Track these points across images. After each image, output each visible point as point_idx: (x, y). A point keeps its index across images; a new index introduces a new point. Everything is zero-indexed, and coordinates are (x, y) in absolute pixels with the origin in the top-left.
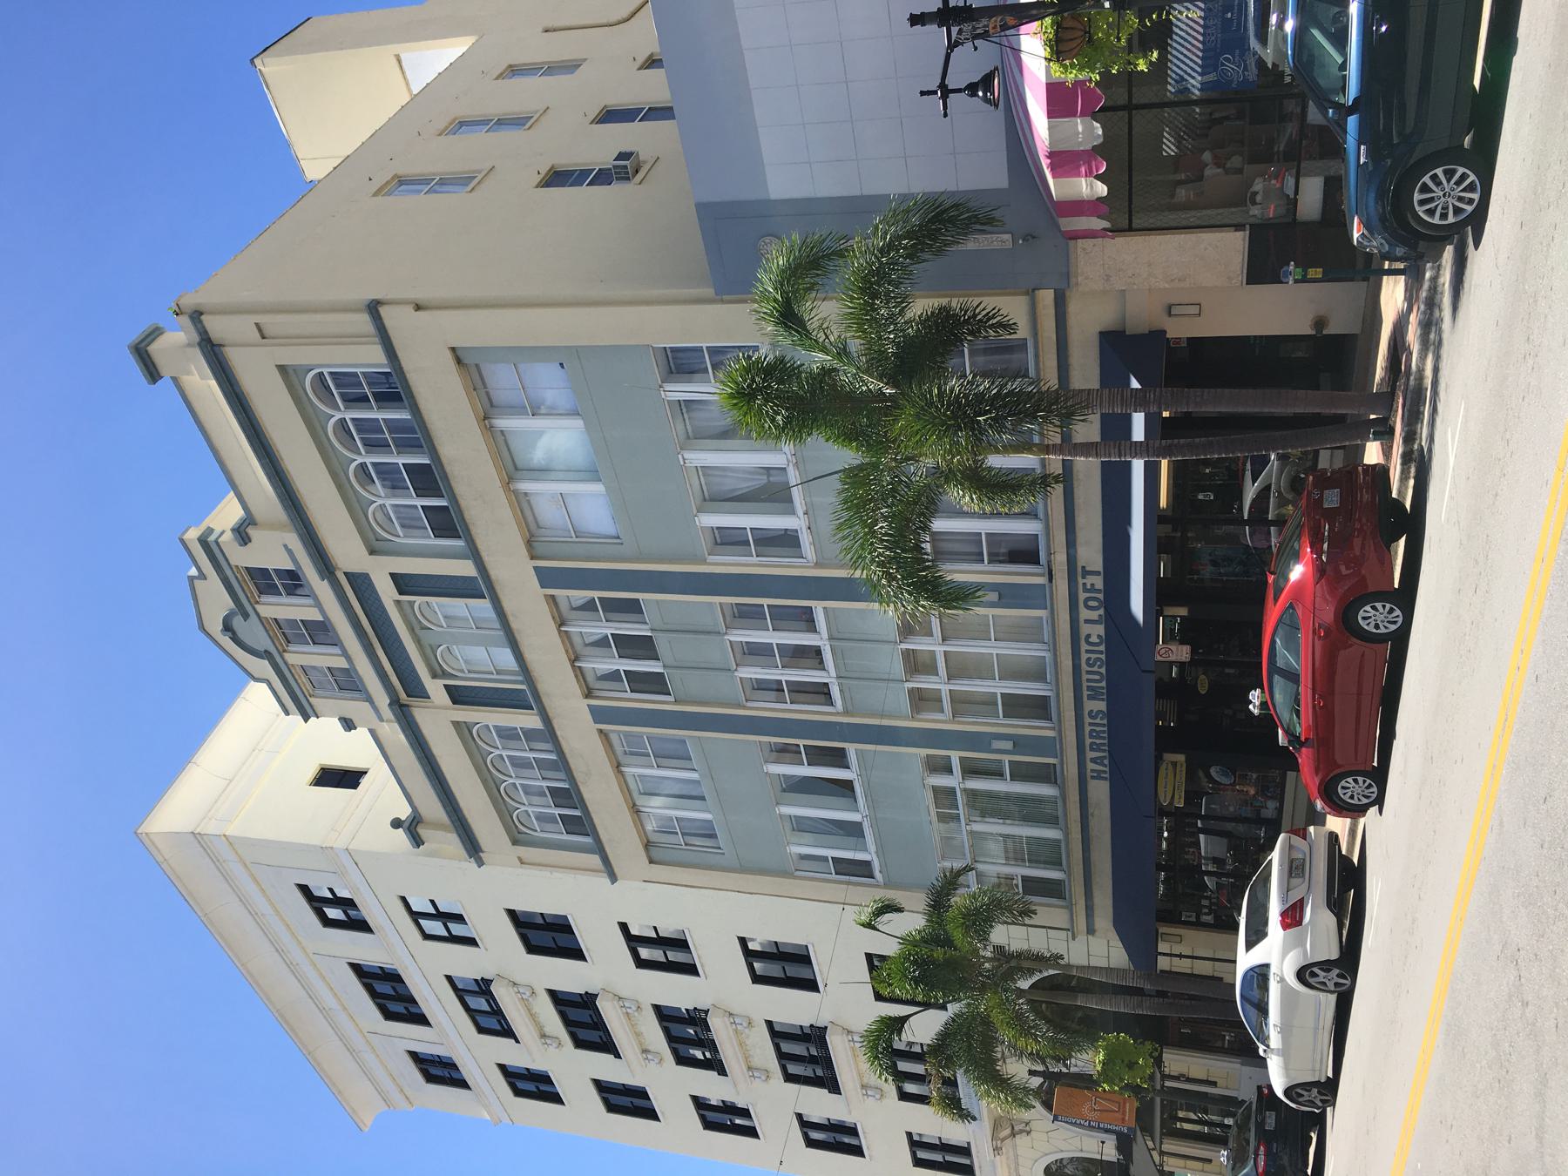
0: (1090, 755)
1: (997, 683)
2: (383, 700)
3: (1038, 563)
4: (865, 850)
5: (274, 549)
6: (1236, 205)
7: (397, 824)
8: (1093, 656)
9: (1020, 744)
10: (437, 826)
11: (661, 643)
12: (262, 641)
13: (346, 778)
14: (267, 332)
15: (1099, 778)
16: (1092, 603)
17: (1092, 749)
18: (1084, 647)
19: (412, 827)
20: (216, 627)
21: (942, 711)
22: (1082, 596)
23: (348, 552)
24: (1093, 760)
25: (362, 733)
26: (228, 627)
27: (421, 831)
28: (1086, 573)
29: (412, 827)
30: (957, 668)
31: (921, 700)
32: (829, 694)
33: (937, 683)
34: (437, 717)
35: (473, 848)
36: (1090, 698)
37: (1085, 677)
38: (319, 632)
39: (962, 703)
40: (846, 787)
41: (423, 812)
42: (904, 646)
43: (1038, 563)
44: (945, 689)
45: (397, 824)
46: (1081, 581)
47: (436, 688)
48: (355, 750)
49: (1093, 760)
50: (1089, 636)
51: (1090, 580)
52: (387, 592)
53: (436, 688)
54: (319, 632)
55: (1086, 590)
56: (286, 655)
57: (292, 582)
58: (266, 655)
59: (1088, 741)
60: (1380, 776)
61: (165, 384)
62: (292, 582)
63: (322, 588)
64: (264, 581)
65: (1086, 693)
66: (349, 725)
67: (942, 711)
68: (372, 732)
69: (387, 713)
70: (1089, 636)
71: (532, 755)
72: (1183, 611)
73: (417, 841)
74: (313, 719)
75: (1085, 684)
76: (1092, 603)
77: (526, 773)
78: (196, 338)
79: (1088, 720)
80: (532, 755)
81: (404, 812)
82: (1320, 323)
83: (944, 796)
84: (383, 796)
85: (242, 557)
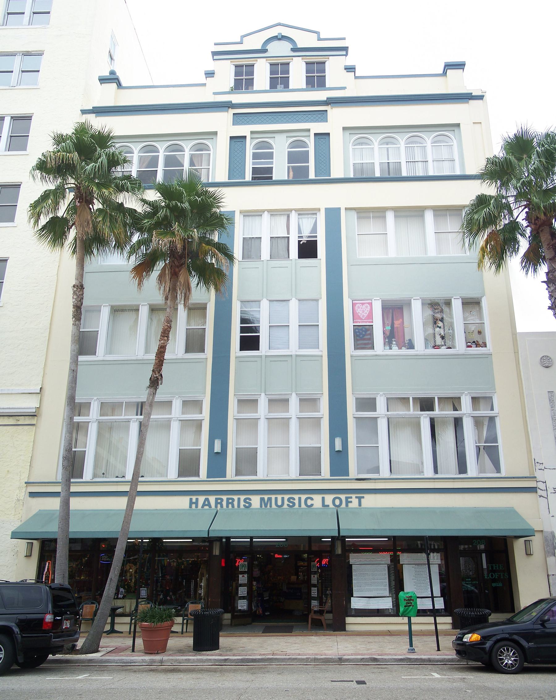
15: (191, 503)
18: (303, 497)
22: (343, 497)
28: (360, 499)
31: (249, 403)
43: (236, 475)
46: (354, 496)
55: (347, 498)
65: (266, 497)
70: (312, 499)
76: (337, 502)
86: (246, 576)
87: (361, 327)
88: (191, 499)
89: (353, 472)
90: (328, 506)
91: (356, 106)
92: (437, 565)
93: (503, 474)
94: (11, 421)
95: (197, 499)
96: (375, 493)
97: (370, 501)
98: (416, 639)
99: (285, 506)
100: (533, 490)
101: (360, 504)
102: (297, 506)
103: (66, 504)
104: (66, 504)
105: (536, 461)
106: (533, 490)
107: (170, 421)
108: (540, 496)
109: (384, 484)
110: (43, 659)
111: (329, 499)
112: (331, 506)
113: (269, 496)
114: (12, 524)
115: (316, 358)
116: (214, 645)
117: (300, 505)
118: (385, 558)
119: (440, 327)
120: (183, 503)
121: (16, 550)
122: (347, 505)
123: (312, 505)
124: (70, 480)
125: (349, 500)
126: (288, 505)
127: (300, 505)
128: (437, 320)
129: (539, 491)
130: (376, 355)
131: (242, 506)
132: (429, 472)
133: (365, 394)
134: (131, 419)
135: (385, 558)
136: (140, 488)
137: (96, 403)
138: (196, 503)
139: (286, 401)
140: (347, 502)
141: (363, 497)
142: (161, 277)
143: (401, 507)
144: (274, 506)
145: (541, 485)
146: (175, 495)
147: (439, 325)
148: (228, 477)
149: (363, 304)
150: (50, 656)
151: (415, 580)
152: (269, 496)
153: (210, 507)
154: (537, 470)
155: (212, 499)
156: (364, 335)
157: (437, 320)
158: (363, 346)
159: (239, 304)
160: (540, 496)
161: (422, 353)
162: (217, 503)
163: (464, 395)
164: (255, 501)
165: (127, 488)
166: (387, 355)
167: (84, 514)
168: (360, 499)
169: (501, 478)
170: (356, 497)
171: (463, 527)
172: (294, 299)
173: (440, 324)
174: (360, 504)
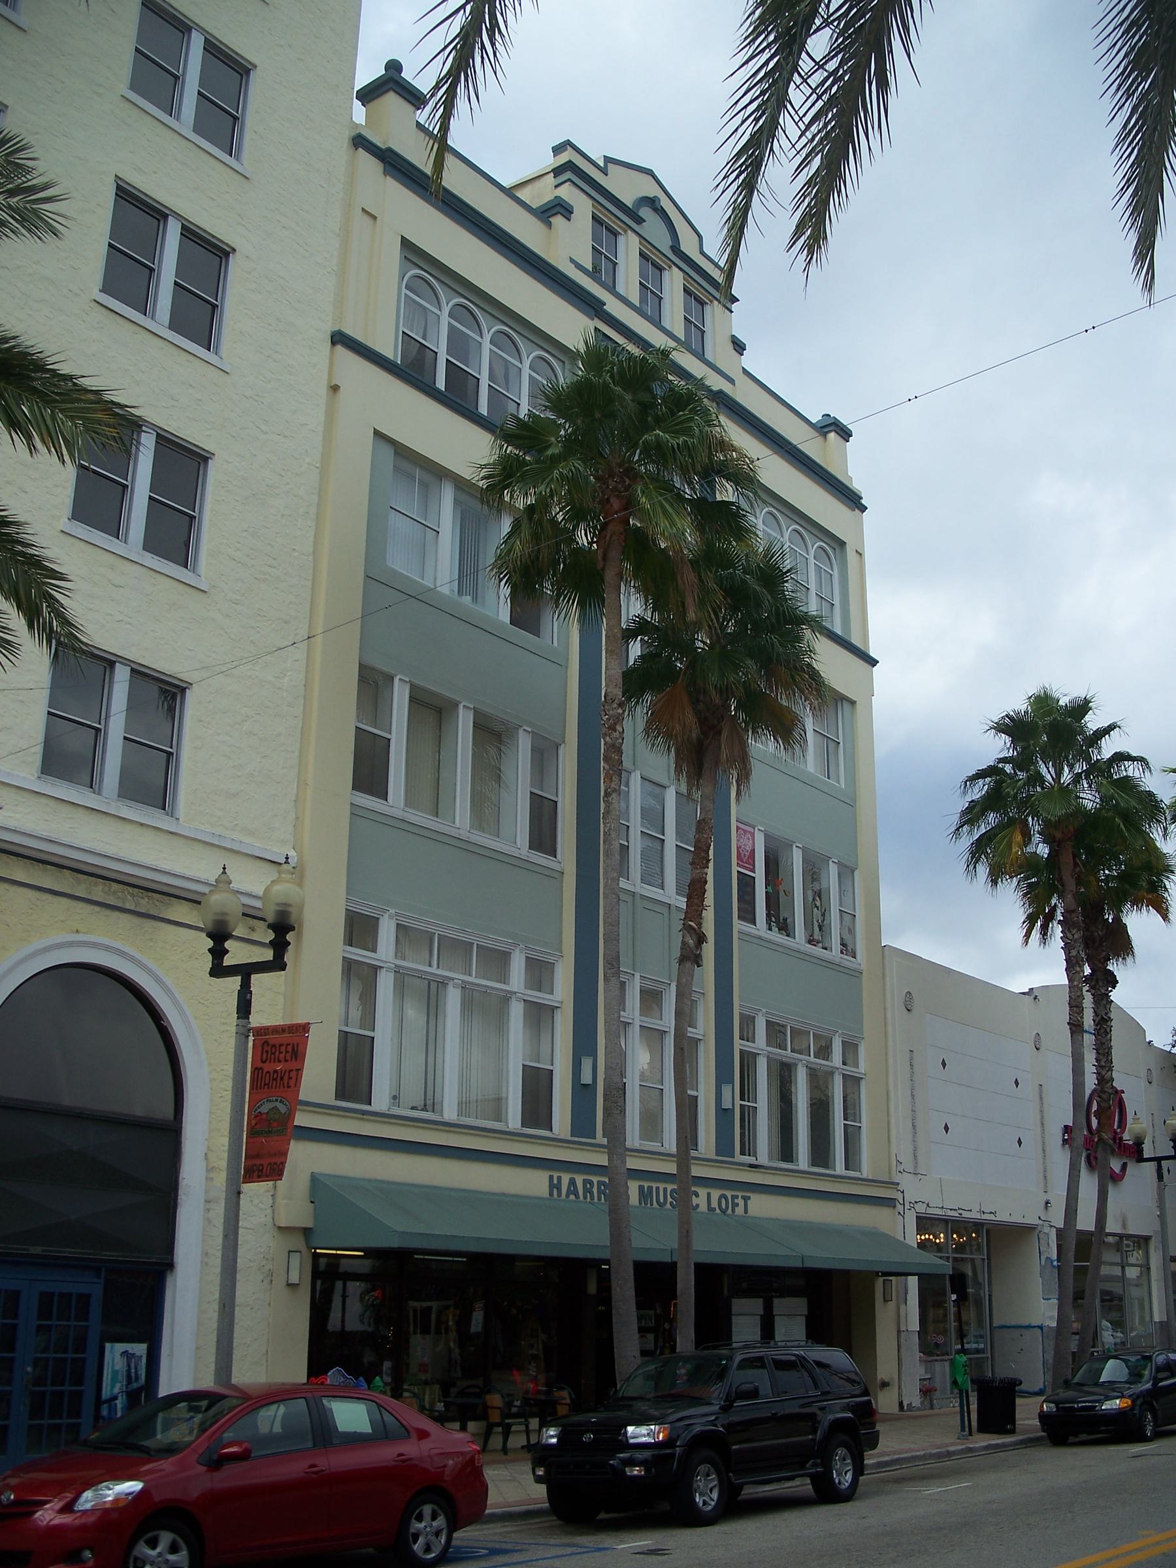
28: (746, 1199)
89: (381, 1100)
91: (761, 441)
93: (866, 1172)
97: (761, 1206)
98: (1030, 1422)
99: (668, 1206)
107: (445, 985)
114: (256, 1202)
115: (659, 908)
120: (535, 1183)
121: (267, 1268)
122: (733, 1211)
124: (688, 1153)
126: (671, 1203)
132: (514, 1118)
134: (453, 979)
138: (559, 1187)
139: (504, 958)
143: (409, 1181)
146: (840, 1201)
155: (579, 1179)
161: (464, 835)
163: (386, 916)
166: (769, 941)
168: (746, 1199)
169: (859, 1179)
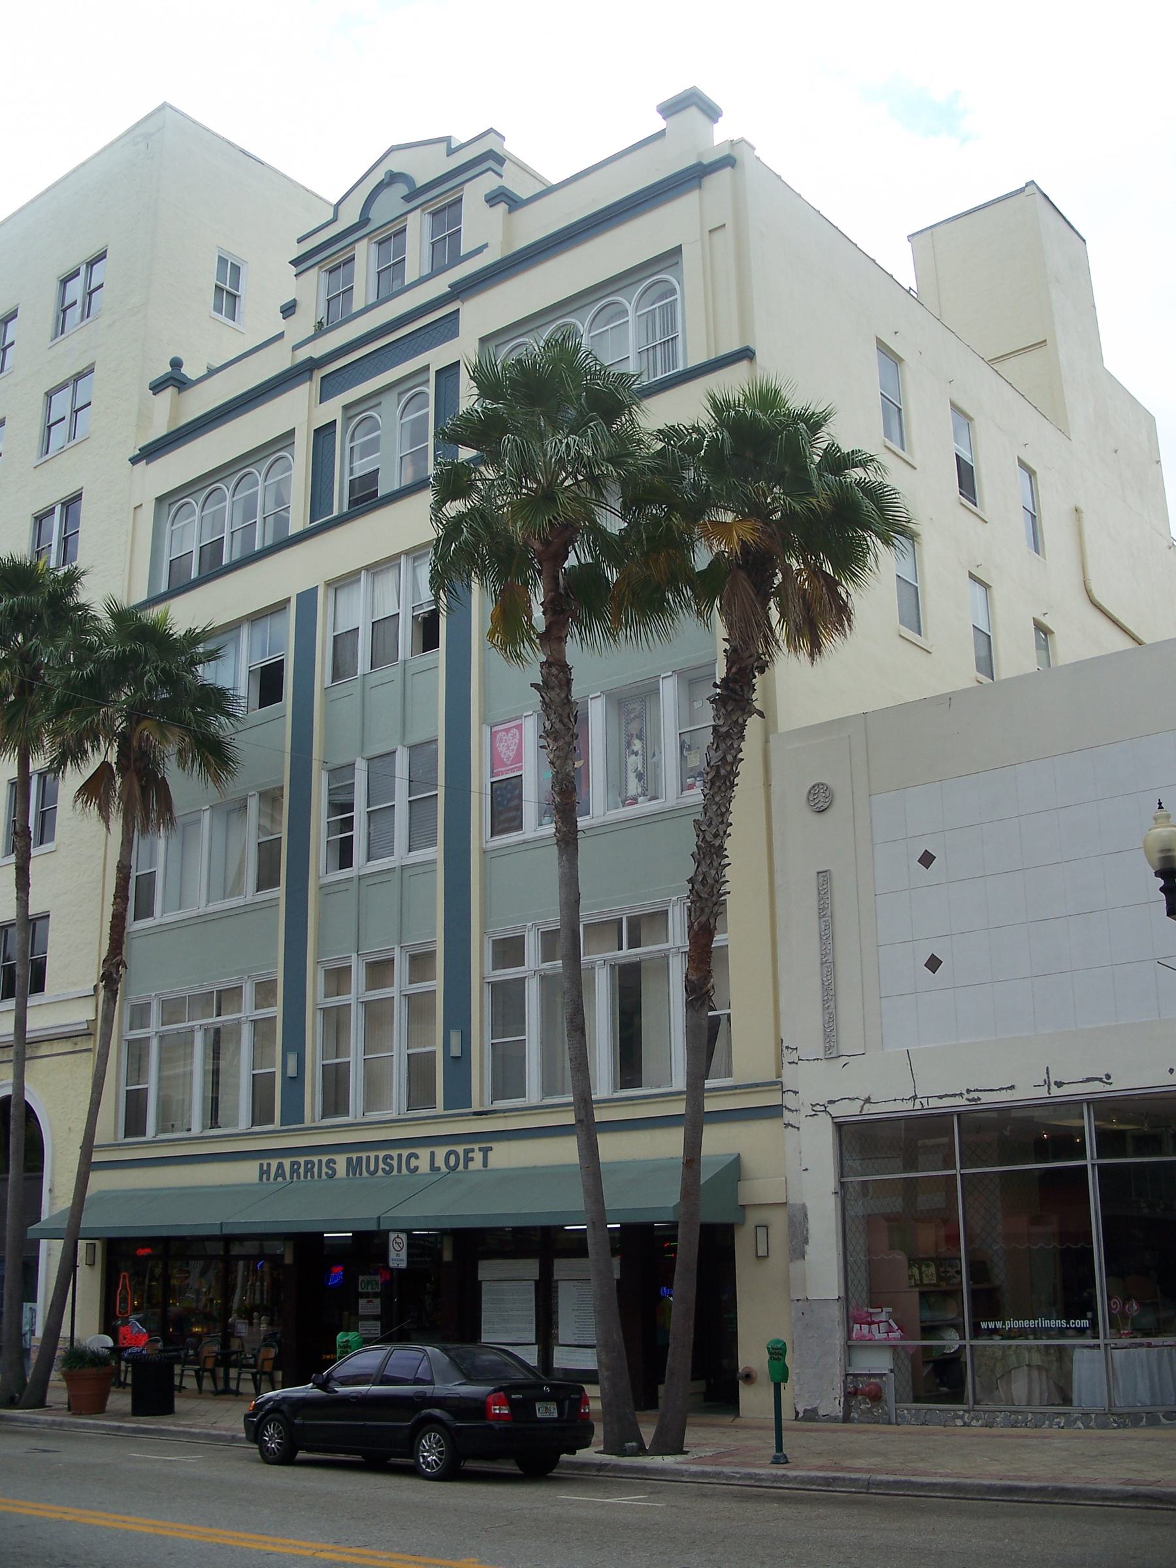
0: (287, 1163)
1: (361, 1057)
2: (318, 349)
3: (495, 1098)
4: (164, 912)
5: (485, 232)
6: (871, 1291)
7: (176, 364)
8: (395, 1163)
9: (294, 1083)
10: (175, 409)
11: (391, 672)
12: (381, 214)
13: (227, 298)
14: (718, 236)
15: (262, 1172)
16: (452, 1159)
17: (293, 1164)
18: (405, 1153)
19: (175, 380)
20: (396, 164)
21: (326, 996)
22: (460, 1149)
23: (483, 315)
24: (280, 1166)
25: (278, 324)
26: (393, 178)
27: (170, 391)
28: (486, 1151)
29: (175, 380)
30: (377, 1014)
31: (338, 978)
32: (232, 895)
33: (357, 991)
34: (298, 411)
35: (150, 452)
36: (349, 1160)
37: (372, 1155)
38: (391, 275)
39: (336, 1020)
40: (345, 860)
41: (190, 394)
42: (669, 690)
43: (495, 1098)
44: (350, 998)
45: (176, 364)
46: (476, 1147)
47: (332, 410)
48: (260, 315)
49: (280, 1166)
50: (417, 1157)
51: (478, 1156)
52: (437, 357)
53: (332, 410)
54: (391, 275)
55: (467, 1152)
56: (366, 240)
57: (447, 248)
58: (364, 221)
59: (302, 1160)
60: (285, 1458)
61: (659, 124)
62: (447, 248)
63: (439, 286)
64: (447, 216)
65: (354, 1156)
66: (288, 310)
67: (326, 996)
68: (281, 336)
69: (303, 354)
70: (417, 1157)
71: (259, 520)
72: (447, 1256)
73: (157, 387)
74: (293, 270)
75: (364, 1155)
76: (452, 1159)
77: (238, 516)
78: (706, 162)
79: (325, 1159)
80: (259, 520)
81: (190, 371)
82: (749, 1377)
83: (226, 998)
84: (214, 348)
85: (474, 193)
86: (377, 1301)
87: (504, 784)
88: (262, 1165)
90: (439, 1168)
92: (533, 1283)
94: (67, 1047)
95: (269, 1165)
96: (123, 1168)
97: (505, 1156)
99: (380, 1173)
100: (774, 1112)
101: (485, 1164)
102: (395, 1172)
103: (590, 1150)
104: (590, 1150)
105: (785, 1044)
106: (774, 1112)
107: (667, 957)
108: (787, 1125)
109: (502, 1121)
110: (554, 1462)
111: (441, 1152)
112: (444, 1169)
113: (359, 1155)
116: (166, 1408)
117: (399, 1170)
118: (530, 1268)
119: (636, 754)
120: (248, 1172)
122: (466, 1166)
123: (417, 1168)
125: (470, 1155)
126: (383, 1169)
127: (399, 1170)
128: (632, 736)
129: (786, 1112)
130: (524, 842)
131: (324, 1176)
133: (505, 931)
135: (530, 1268)
136: (710, 1105)
137: (677, 909)
138: (268, 1172)
140: (468, 1160)
141: (491, 1149)
142: (182, 764)
144: (365, 1174)
145: (790, 1100)
147: (635, 748)
148: (308, 1123)
149: (507, 730)
150: (564, 1457)
151: (576, 1313)
152: (359, 1155)
153: (284, 1178)
154: (786, 1065)
156: (509, 800)
157: (632, 736)
158: (506, 825)
159: (325, 776)
160: (787, 1125)
162: (292, 1172)
164: (341, 1161)
165: (679, 1108)
167: (106, 1197)
170: (480, 1149)
171: (305, 1217)
172: (400, 748)
173: (637, 745)
174: (485, 1164)
